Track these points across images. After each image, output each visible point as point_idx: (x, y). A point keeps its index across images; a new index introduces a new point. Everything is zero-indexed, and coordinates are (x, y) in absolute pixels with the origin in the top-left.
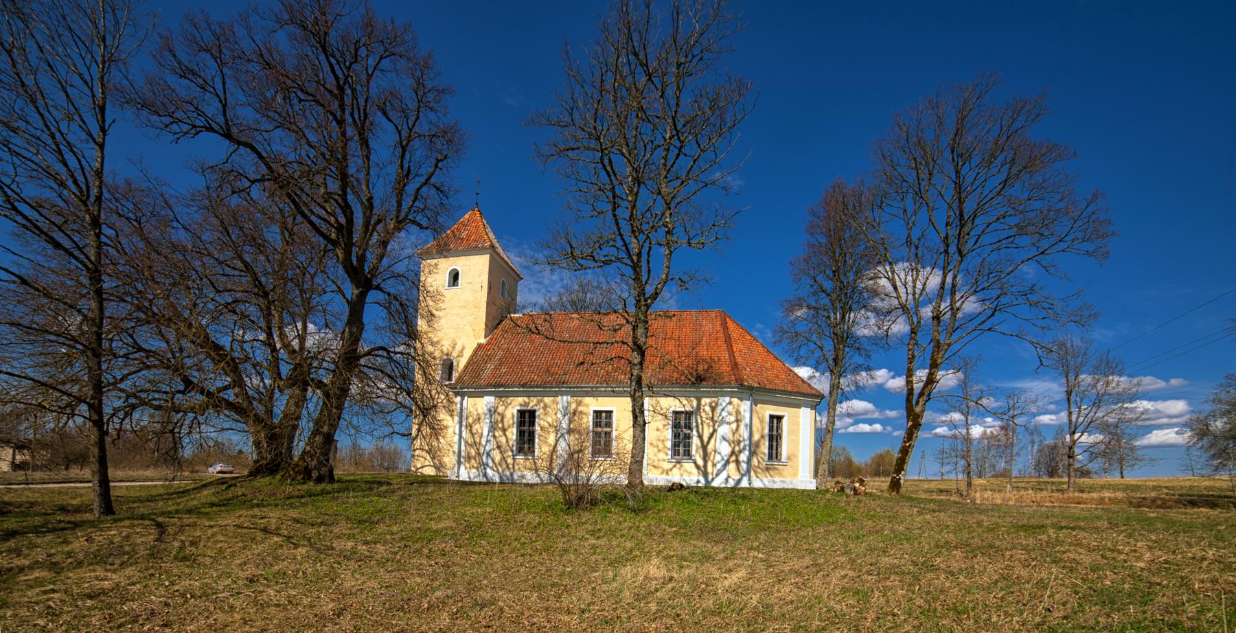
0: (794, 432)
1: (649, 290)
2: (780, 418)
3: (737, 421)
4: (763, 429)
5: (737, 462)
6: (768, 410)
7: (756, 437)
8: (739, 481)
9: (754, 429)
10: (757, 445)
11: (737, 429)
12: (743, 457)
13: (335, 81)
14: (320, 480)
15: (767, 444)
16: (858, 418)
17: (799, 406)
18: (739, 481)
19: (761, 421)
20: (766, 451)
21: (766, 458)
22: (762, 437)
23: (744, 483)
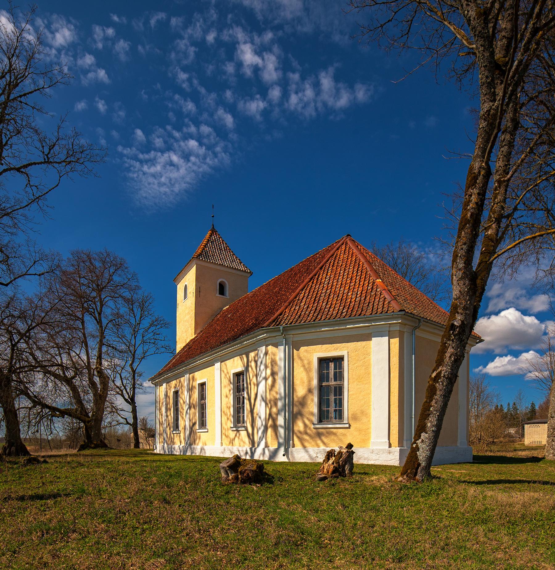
0: (365, 377)
1: (22, 170)
2: (339, 360)
3: (273, 374)
4: (310, 381)
5: (275, 427)
6: (313, 354)
7: (300, 391)
8: (275, 453)
9: (297, 382)
10: (303, 402)
11: (273, 386)
12: (281, 421)
13: (551, 348)
14: (96, 447)
15: (316, 400)
16: (515, 344)
17: (367, 337)
18: (275, 453)
19: (308, 370)
20: (315, 410)
21: (315, 419)
22: (310, 391)
23: (281, 458)
